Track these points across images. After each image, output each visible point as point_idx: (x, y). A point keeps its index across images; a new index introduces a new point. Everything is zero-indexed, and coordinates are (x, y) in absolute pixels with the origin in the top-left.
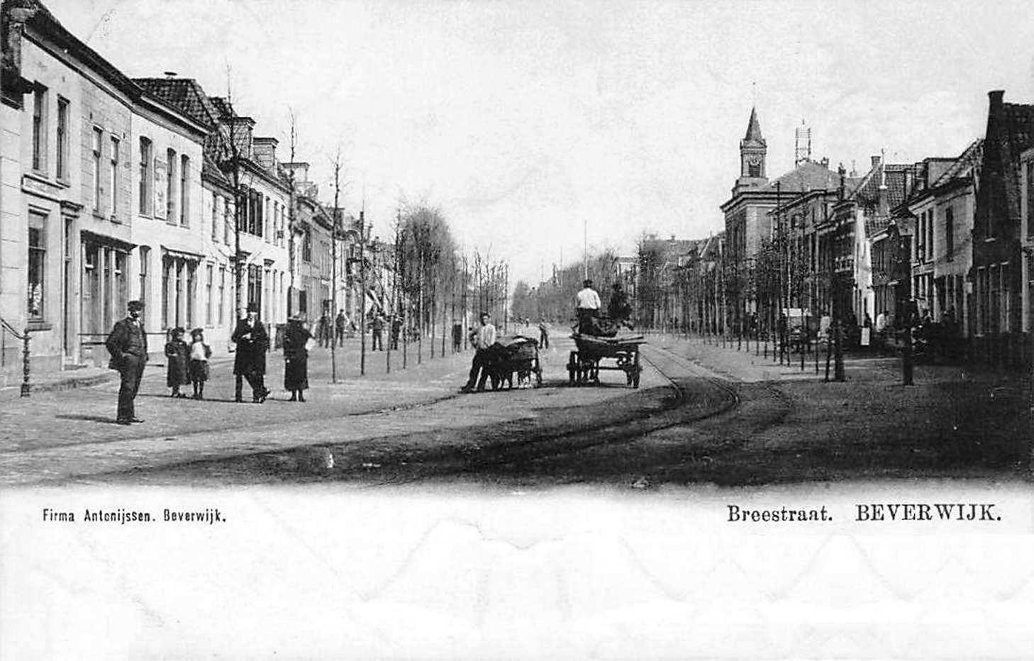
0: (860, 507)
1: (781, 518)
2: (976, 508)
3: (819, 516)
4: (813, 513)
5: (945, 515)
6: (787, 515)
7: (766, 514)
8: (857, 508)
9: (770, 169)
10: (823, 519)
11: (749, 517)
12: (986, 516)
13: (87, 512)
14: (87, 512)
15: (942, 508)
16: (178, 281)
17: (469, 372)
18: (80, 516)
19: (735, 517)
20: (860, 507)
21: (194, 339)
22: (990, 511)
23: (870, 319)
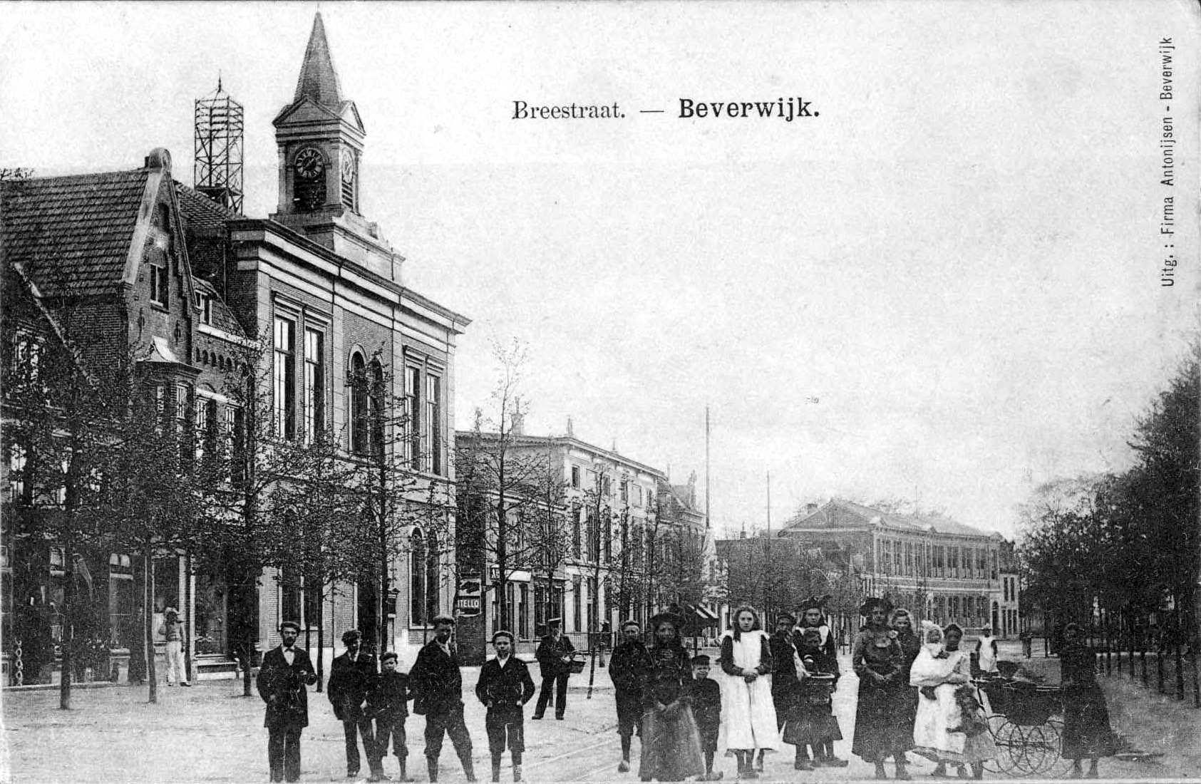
0: (517, 103)
1: (571, 114)
2: (519, 104)
3: (612, 111)
4: (605, 109)
5: (765, 114)
6: (577, 111)
7: (702, 107)
8: (515, 104)
9: (264, 620)
10: (615, 116)
11: (537, 113)
12: (803, 113)
13: (1163, 182)
14: (1163, 182)
15: (762, 107)
16: (1167, 94)
17: (475, 686)
18: (1167, 191)
19: (687, 112)
20: (517, 103)
21: (396, 398)
22: (807, 108)
23: (976, 701)
